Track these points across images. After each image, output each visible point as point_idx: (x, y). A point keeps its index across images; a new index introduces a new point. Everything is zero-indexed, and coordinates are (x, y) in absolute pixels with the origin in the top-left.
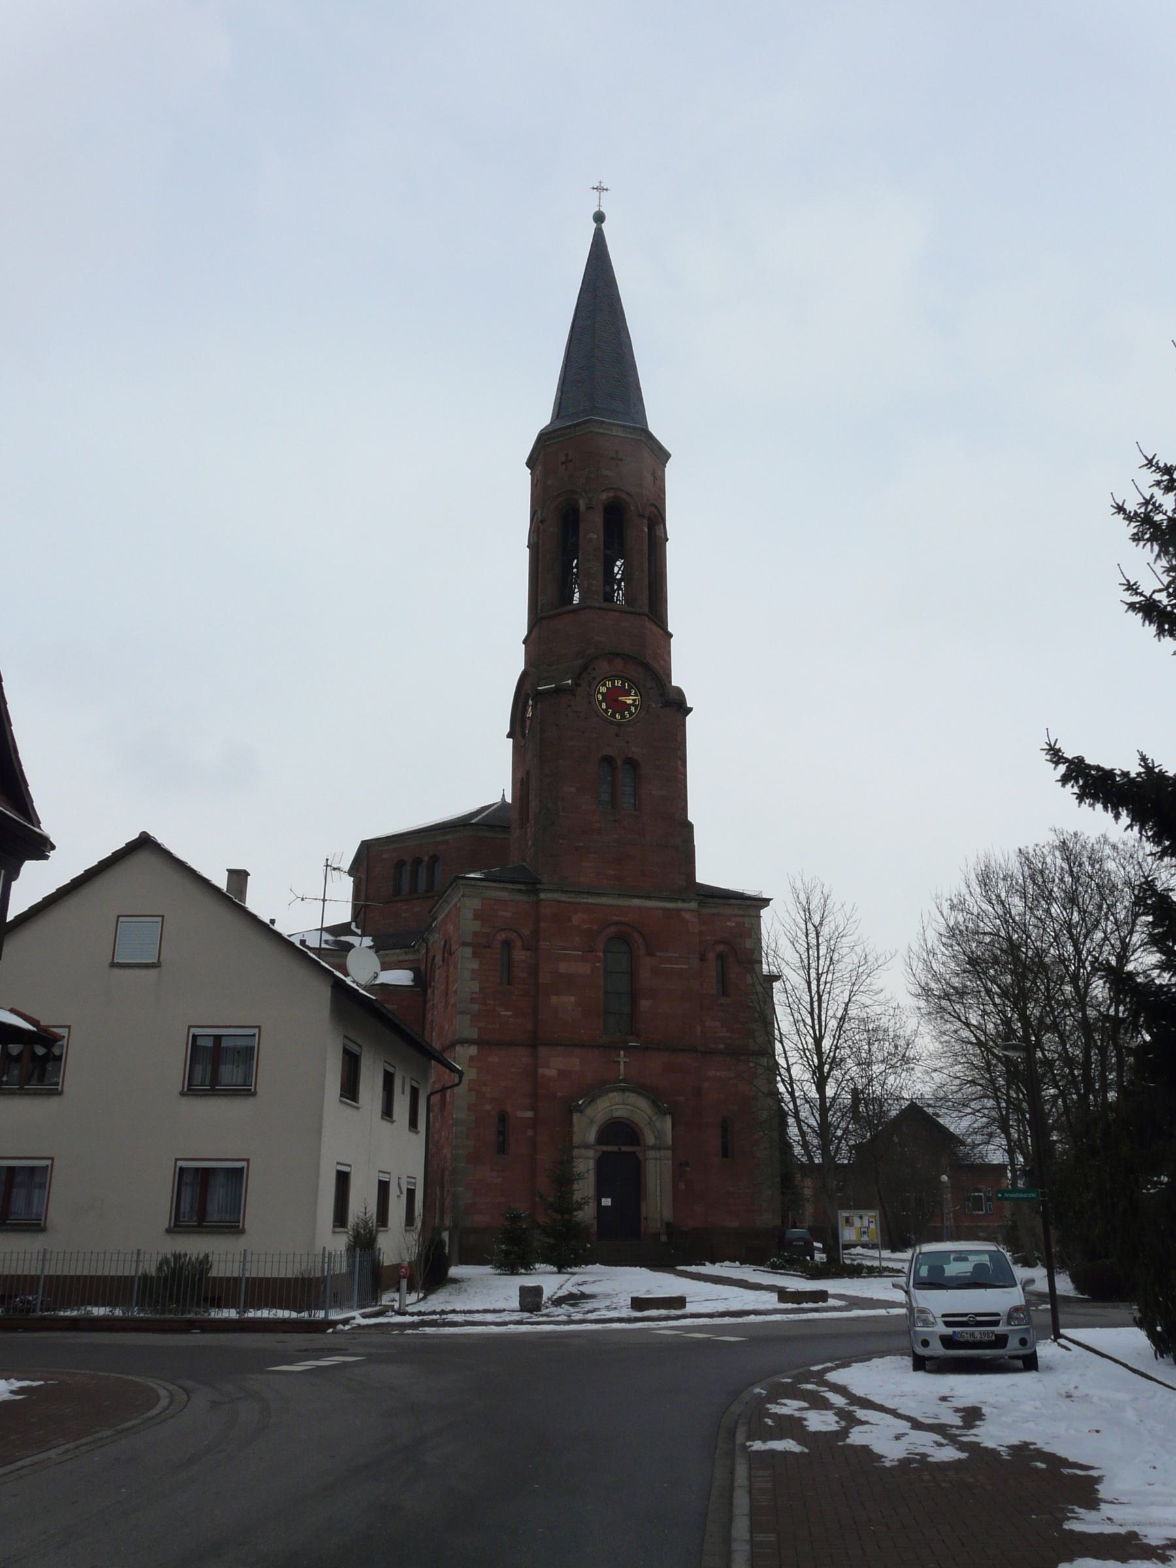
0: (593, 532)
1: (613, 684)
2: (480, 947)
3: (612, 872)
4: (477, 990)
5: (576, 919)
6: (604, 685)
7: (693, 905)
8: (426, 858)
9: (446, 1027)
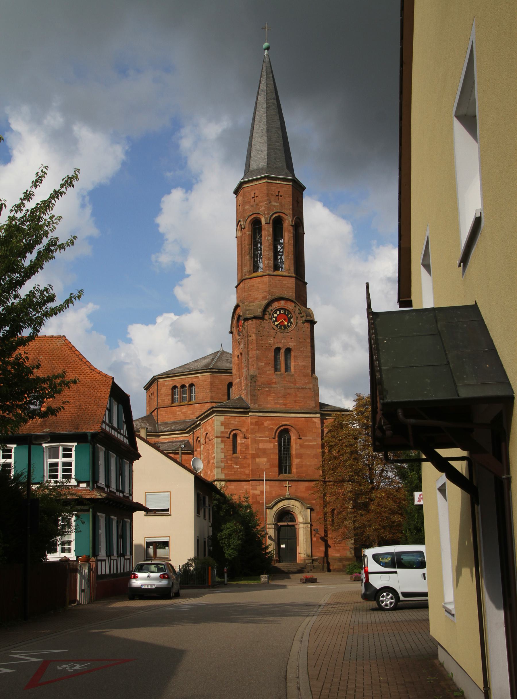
1: (280, 312)
2: (222, 438)
3: (281, 402)
4: (224, 457)
5: (266, 424)
6: (276, 313)
8: (187, 385)
9: (209, 472)
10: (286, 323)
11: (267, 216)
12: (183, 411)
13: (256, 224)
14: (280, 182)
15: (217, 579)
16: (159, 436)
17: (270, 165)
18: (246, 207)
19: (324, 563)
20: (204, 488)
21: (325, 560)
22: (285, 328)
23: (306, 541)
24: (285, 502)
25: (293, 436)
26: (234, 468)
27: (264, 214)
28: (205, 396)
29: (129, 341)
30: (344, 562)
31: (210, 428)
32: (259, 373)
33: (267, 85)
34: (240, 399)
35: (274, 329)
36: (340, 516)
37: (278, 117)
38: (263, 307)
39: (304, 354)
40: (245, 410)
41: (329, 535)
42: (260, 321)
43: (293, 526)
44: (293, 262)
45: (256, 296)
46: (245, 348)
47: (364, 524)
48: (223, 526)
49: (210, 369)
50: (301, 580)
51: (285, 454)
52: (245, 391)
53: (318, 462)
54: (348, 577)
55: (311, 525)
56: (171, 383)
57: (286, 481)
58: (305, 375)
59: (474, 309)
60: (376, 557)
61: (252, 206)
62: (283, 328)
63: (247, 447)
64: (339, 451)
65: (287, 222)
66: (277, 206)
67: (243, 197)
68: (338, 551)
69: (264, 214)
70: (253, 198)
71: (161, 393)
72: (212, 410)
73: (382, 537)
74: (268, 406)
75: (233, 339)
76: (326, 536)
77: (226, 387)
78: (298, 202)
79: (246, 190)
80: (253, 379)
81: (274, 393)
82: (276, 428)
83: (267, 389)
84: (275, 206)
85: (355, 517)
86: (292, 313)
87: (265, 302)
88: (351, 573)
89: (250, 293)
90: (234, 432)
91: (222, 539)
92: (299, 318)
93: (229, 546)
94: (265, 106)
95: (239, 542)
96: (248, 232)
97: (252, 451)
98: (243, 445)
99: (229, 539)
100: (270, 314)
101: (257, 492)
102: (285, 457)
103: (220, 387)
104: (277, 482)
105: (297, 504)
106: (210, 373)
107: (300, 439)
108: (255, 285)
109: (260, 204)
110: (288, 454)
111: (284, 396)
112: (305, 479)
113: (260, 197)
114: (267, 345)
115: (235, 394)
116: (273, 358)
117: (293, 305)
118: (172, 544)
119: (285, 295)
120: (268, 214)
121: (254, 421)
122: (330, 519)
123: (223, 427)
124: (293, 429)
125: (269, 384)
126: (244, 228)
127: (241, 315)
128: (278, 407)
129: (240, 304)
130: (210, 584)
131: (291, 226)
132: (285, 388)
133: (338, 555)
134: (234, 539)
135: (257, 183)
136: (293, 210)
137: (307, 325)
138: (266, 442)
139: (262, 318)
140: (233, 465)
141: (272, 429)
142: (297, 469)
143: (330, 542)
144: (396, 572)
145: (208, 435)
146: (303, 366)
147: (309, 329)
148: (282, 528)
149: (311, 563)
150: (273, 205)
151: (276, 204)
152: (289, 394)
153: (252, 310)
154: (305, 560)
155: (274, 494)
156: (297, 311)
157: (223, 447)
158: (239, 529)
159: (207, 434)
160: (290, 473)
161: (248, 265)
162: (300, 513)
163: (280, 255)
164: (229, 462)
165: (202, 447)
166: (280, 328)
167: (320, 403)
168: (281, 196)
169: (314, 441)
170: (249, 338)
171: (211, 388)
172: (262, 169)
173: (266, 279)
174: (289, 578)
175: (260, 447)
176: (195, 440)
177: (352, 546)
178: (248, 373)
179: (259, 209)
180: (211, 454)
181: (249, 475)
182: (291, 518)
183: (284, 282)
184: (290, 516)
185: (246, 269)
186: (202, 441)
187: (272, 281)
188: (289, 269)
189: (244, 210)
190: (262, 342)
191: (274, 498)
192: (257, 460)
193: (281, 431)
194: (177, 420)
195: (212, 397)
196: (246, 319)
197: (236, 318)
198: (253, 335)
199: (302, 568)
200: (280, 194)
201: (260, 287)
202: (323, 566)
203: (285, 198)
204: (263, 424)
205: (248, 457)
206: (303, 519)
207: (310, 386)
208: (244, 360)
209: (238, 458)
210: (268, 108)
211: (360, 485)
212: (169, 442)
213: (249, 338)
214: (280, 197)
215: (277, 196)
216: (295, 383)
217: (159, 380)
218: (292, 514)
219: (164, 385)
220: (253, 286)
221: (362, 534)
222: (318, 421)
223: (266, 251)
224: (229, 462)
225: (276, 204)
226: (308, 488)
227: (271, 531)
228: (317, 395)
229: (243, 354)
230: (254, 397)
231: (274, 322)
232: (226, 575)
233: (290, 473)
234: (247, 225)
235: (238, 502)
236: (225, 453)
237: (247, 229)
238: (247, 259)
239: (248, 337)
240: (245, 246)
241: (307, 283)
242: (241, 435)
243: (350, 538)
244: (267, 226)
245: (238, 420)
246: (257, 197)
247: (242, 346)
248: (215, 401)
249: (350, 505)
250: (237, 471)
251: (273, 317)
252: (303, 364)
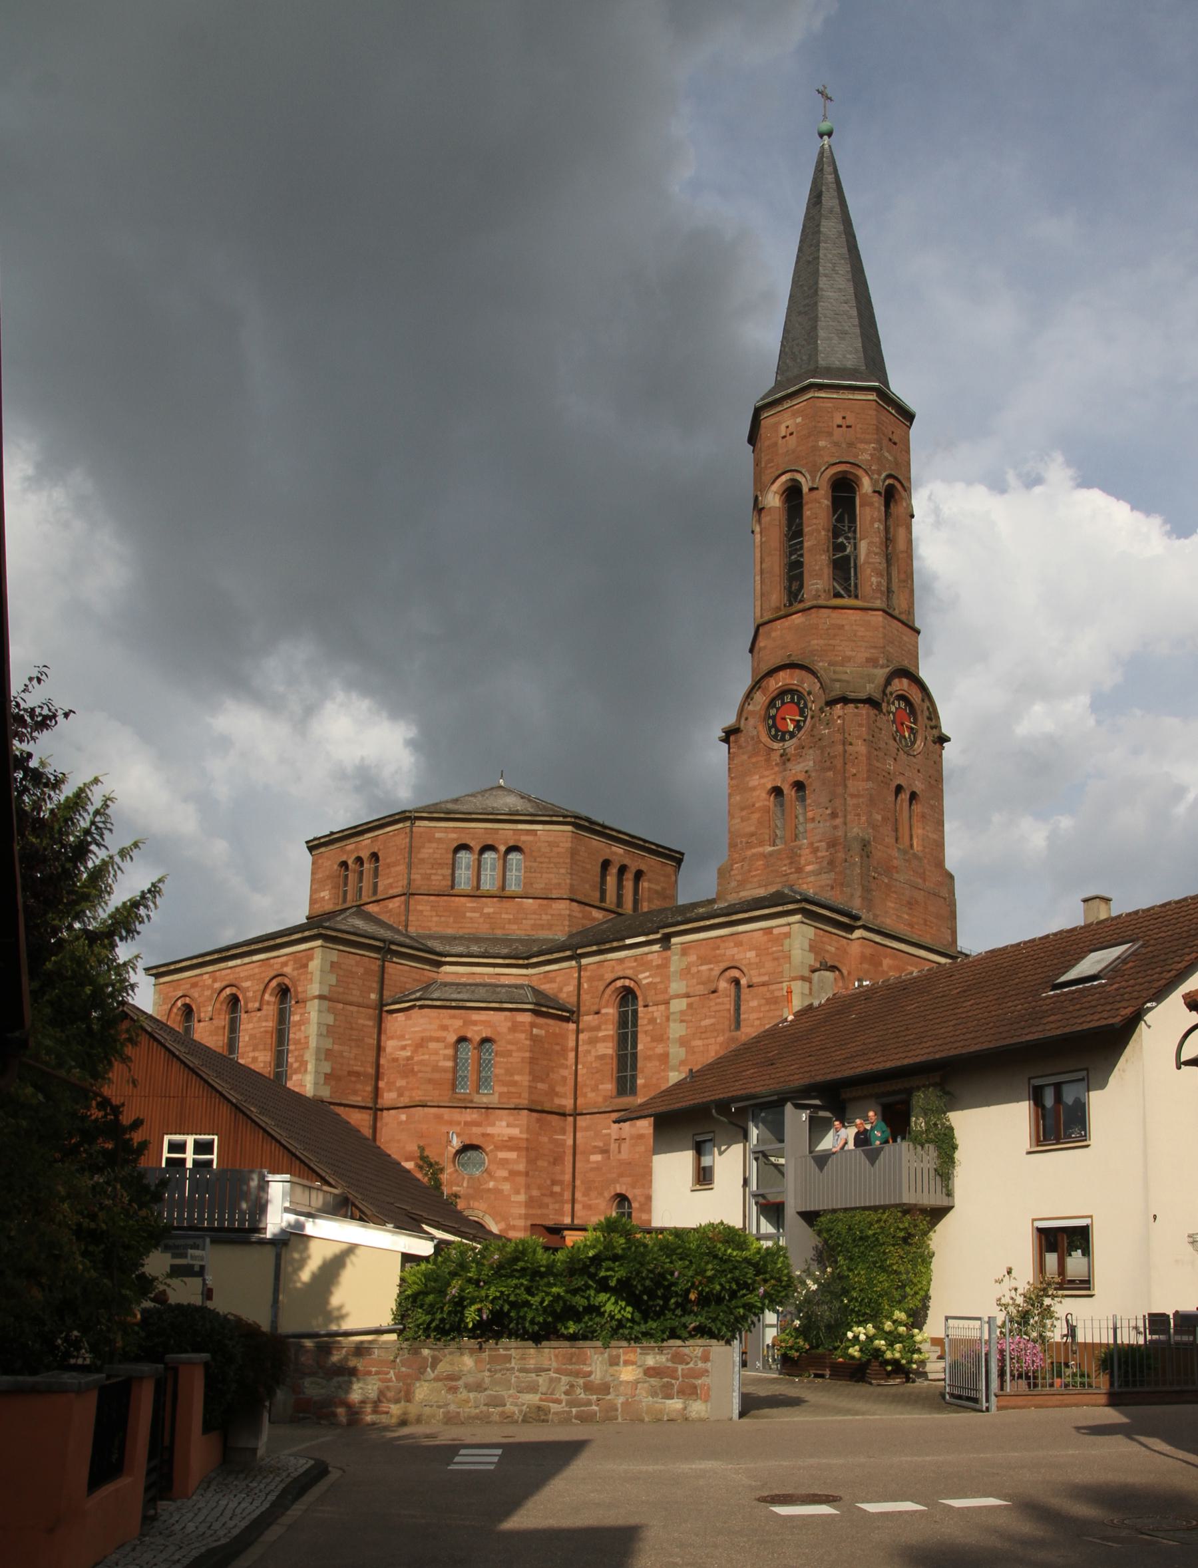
12: (486, 910)
16: (440, 964)
28: (555, 881)
45: (849, 653)
56: (454, 836)
61: (836, 444)
71: (421, 856)
79: (819, 403)
83: (886, 881)
89: (832, 642)
103: (589, 866)
106: (569, 828)
108: (847, 628)
128: (902, 929)
153: (848, 682)
194: (466, 931)
195: (572, 888)
201: (859, 634)
212: (471, 985)
217: (418, 823)
219: (431, 839)
230: (868, 902)
237: (822, 492)
246: (791, 434)
248: (578, 898)
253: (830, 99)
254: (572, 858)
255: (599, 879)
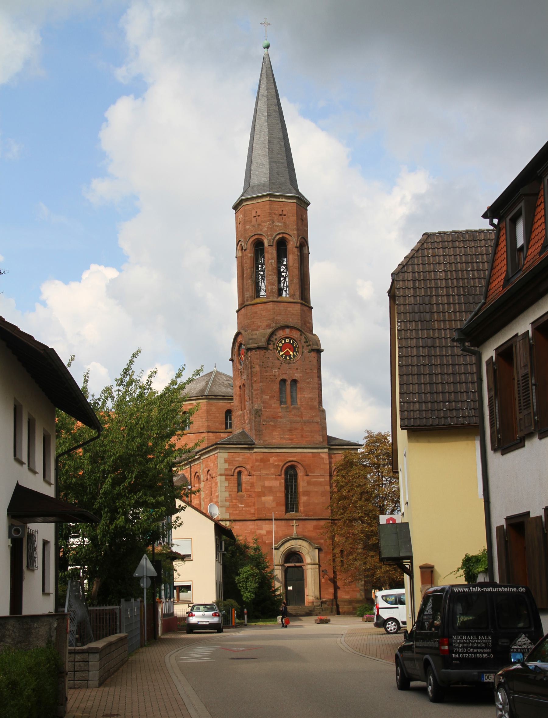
0: (271, 253)
1: (285, 341)
3: (287, 436)
5: (272, 460)
6: (281, 342)
7: (326, 450)
10: (291, 353)
11: (270, 238)
13: (258, 247)
14: (283, 200)
15: (237, 621)
17: (273, 181)
18: (248, 227)
19: (332, 605)
20: (222, 533)
21: (334, 603)
22: (290, 358)
23: (314, 583)
24: (292, 542)
25: (300, 473)
26: (239, 507)
27: (267, 235)
28: (201, 425)
29: (44, 304)
30: (354, 604)
31: (212, 464)
32: (264, 407)
33: (267, 89)
34: (243, 433)
35: (279, 360)
36: (351, 557)
37: (280, 126)
38: (267, 336)
39: (311, 386)
40: (250, 446)
41: (338, 577)
42: (264, 351)
43: (301, 567)
44: (298, 287)
45: (259, 324)
46: (248, 379)
47: (375, 566)
48: (241, 570)
49: (206, 396)
50: (316, 621)
51: (292, 492)
52: (249, 425)
53: (325, 500)
54: (360, 619)
55: (320, 566)
57: (293, 520)
58: (312, 408)
59: (408, 523)
60: (385, 598)
61: (253, 226)
62: (288, 358)
63: (252, 485)
64: (349, 491)
65: (291, 243)
66: (281, 226)
67: (244, 216)
68: (348, 593)
69: (267, 235)
70: (254, 217)
72: (215, 447)
73: (393, 579)
74: (274, 441)
75: (233, 367)
76: (335, 577)
77: (224, 415)
78: (303, 220)
79: (246, 208)
80: (258, 413)
81: (279, 427)
82: (283, 464)
84: (278, 226)
85: (366, 558)
86: (298, 342)
87: (269, 331)
88: (361, 615)
90: (238, 469)
91: (240, 583)
92: (305, 347)
93: (247, 589)
94: (266, 114)
95: (257, 585)
96: (250, 254)
97: (258, 489)
98: (248, 483)
99: (247, 582)
100: (274, 344)
101: (263, 532)
102: (292, 495)
104: (283, 521)
105: (305, 544)
106: (205, 400)
107: (307, 475)
109: (263, 224)
110: (295, 492)
111: (290, 430)
112: (313, 518)
113: (262, 217)
114: (271, 377)
115: (236, 427)
116: (278, 390)
117: (299, 333)
118: (193, 588)
119: (290, 323)
120: (271, 235)
121: (259, 457)
122: (339, 559)
123: (227, 464)
124: (299, 466)
125: (274, 418)
126: (245, 250)
127: (243, 343)
129: (243, 332)
130: (233, 624)
131: (296, 247)
132: (291, 422)
133: (347, 597)
134: (251, 582)
135: (259, 201)
136: (298, 230)
137: (313, 354)
138: (273, 479)
139: (266, 348)
140: (237, 504)
141: (278, 465)
142: (304, 507)
143: (339, 584)
144: (398, 608)
145: (210, 472)
146: (310, 398)
147: (316, 359)
148: (289, 569)
149: (319, 606)
150: (276, 226)
151: (279, 224)
152: (296, 429)
153: (255, 339)
154: (313, 602)
155: (281, 534)
156: (303, 340)
157: (227, 485)
158: (256, 573)
159: (209, 470)
160: (297, 511)
161: (250, 291)
162: (308, 553)
163: (283, 276)
164: (233, 501)
165: (203, 483)
166: (285, 358)
167: (328, 436)
168: (285, 215)
169: (321, 477)
170: (253, 369)
171: (207, 416)
172: (264, 185)
173: (270, 306)
174: (301, 620)
175: (266, 485)
176: (193, 475)
177: (363, 588)
178: (253, 407)
179: (261, 230)
180: (213, 492)
181: (254, 514)
182: (298, 558)
183: (289, 309)
184: (298, 556)
185: (248, 294)
186: (203, 477)
187: (276, 308)
188: (294, 295)
189: (245, 230)
190: (268, 374)
191: (281, 538)
192: (263, 498)
193: (287, 468)
195: (208, 427)
196: (249, 349)
197: (237, 345)
198: (257, 366)
199: (311, 611)
200: (284, 213)
202: (332, 608)
203: (289, 218)
204: (269, 460)
205: (253, 495)
206: (311, 560)
207: (317, 419)
208: (247, 392)
209: (242, 497)
210: (269, 116)
211: (371, 526)
213: (253, 369)
214: (283, 216)
215: (280, 215)
216: (301, 416)
218: (299, 555)
220: (256, 313)
221: (373, 575)
222: (325, 456)
223: (270, 275)
224: (233, 501)
225: (279, 224)
226: (316, 528)
227: (278, 573)
228: (324, 428)
229: (246, 386)
230: (259, 433)
231: (279, 352)
232: (246, 616)
233: (297, 511)
234: (249, 246)
235: (243, 543)
236: (229, 492)
237: (248, 251)
238: (249, 283)
239: (251, 368)
240: (247, 269)
241: (312, 308)
242: (246, 473)
243: (361, 579)
244: (270, 249)
245: (243, 457)
247: (244, 377)
248: (212, 430)
249: (360, 546)
250: (242, 510)
251: (278, 347)
252: (310, 396)
253: (262, 24)
254: (207, 414)
255: (224, 420)
